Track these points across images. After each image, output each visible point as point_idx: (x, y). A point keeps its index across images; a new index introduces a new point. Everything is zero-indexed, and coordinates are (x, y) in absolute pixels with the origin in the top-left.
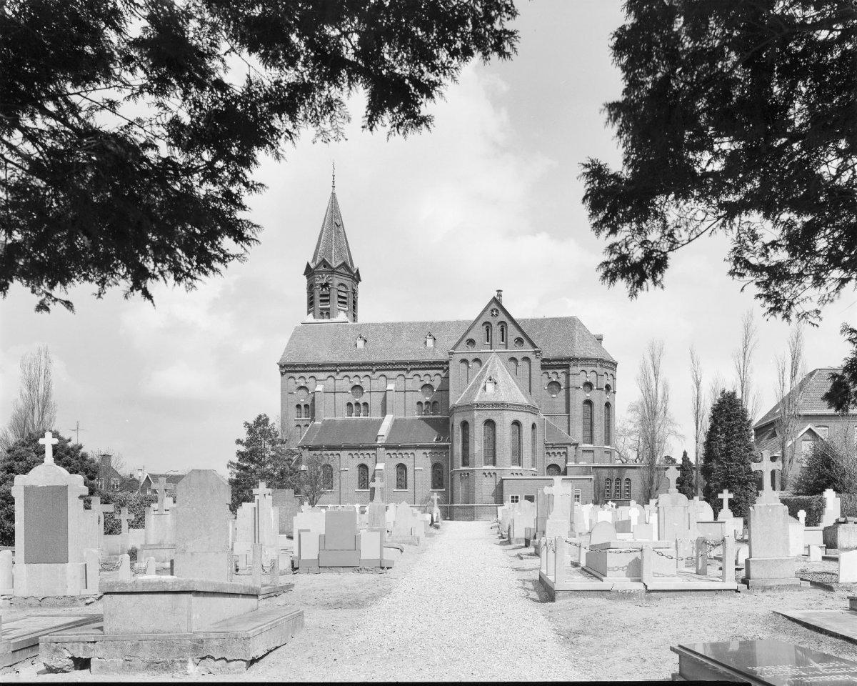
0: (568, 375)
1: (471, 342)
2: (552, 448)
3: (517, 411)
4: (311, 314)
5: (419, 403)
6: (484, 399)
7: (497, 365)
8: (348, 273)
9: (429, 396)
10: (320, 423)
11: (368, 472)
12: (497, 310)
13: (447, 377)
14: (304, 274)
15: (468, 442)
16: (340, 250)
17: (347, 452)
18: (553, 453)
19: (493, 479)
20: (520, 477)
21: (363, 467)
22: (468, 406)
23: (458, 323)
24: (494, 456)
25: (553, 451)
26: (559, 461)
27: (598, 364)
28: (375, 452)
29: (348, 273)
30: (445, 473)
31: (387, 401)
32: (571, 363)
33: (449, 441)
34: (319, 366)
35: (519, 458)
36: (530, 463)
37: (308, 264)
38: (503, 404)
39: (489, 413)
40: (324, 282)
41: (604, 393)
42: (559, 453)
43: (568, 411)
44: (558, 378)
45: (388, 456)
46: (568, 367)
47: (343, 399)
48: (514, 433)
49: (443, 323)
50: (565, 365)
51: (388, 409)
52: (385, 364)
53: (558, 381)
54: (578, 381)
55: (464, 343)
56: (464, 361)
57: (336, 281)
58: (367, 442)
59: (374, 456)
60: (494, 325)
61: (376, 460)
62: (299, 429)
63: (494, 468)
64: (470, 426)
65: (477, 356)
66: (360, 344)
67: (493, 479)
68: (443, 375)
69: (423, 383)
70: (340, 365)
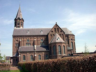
1: (52, 31)
7: (57, 36)
43: (68, 43)
46: (68, 36)
52: (34, 35)
55: (51, 31)
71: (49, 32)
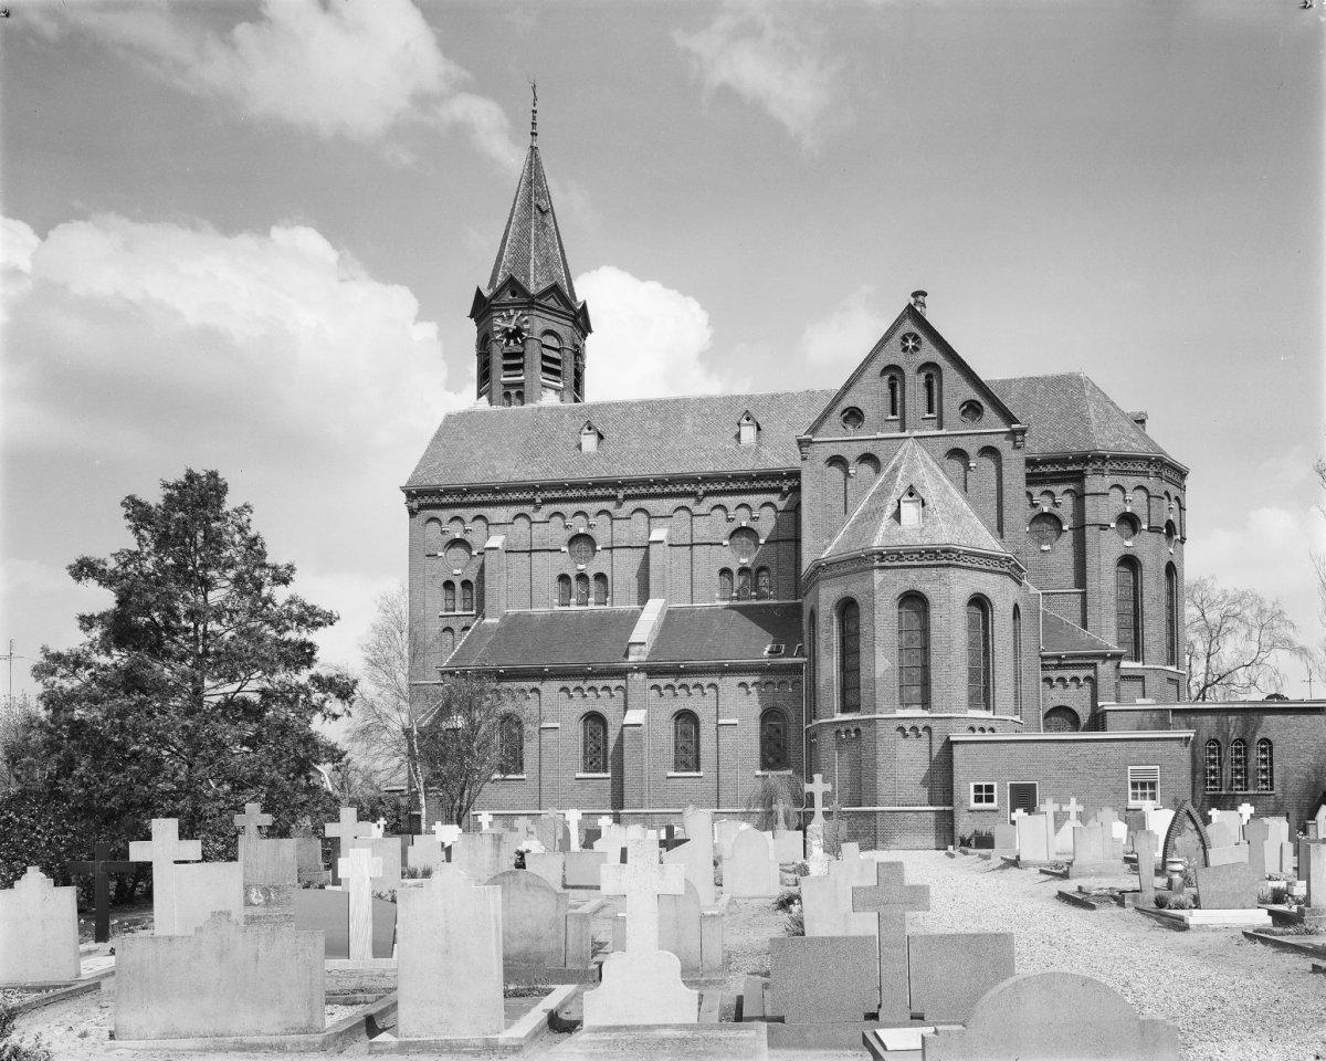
0: (1079, 497)
1: (854, 415)
2: (1057, 667)
3: (981, 570)
4: (484, 398)
5: (725, 572)
6: (898, 541)
8: (563, 309)
9: (748, 554)
10: (496, 621)
11: (605, 731)
12: (916, 338)
13: (795, 509)
14: (471, 317)
15: (857, 652)
16: (547, 261)
17: (557, 684)
18: (1062, 680)
19: (923, 743)
20: (988, 736)
21: (595, 719)
22: (857, 559)
23: (811, 396)
24: (926, 684)
25: (1060, 673)
26: (1078, 700)
27: (1152, 470)
28: (622, 683)
29: (563, 309)
30: (792, 733)
31: (651, 568)
32: (1089, 469)
33: (801, 653)
34: (495, 492)
35: (987, 689)
36: (1011, 705)
37: (478, 290)
38: (946, 551)
39: (913, 574)
40: (512, 326)
41: (1163, 537)
42: (1075, 679)
43: (1081, 579)
44: (1056, 505)
45: (655, 692)
46: (1079, 477)
47: (548, 568)
48: (972, 626)
49: (774, 397)
50: (1074, 472)
51: (652, 586)
52: (646, 483)
53: (1056, 511)
54: (1105, 509)
55: (836, 417)
56: (837, 461)
57: (537, 324)
58: (601, 659)
59: (619, 694)
60: (910, 372)
61: (626, 703)
62: (448, 635)
63: (926, 714)
64: (863, 609)
65: (868, 448)
66: (589, 442)
67: (923, 743)
68: (781, 505)
69: (734, 525)
70: (543, 488)
71: (814, 430)
